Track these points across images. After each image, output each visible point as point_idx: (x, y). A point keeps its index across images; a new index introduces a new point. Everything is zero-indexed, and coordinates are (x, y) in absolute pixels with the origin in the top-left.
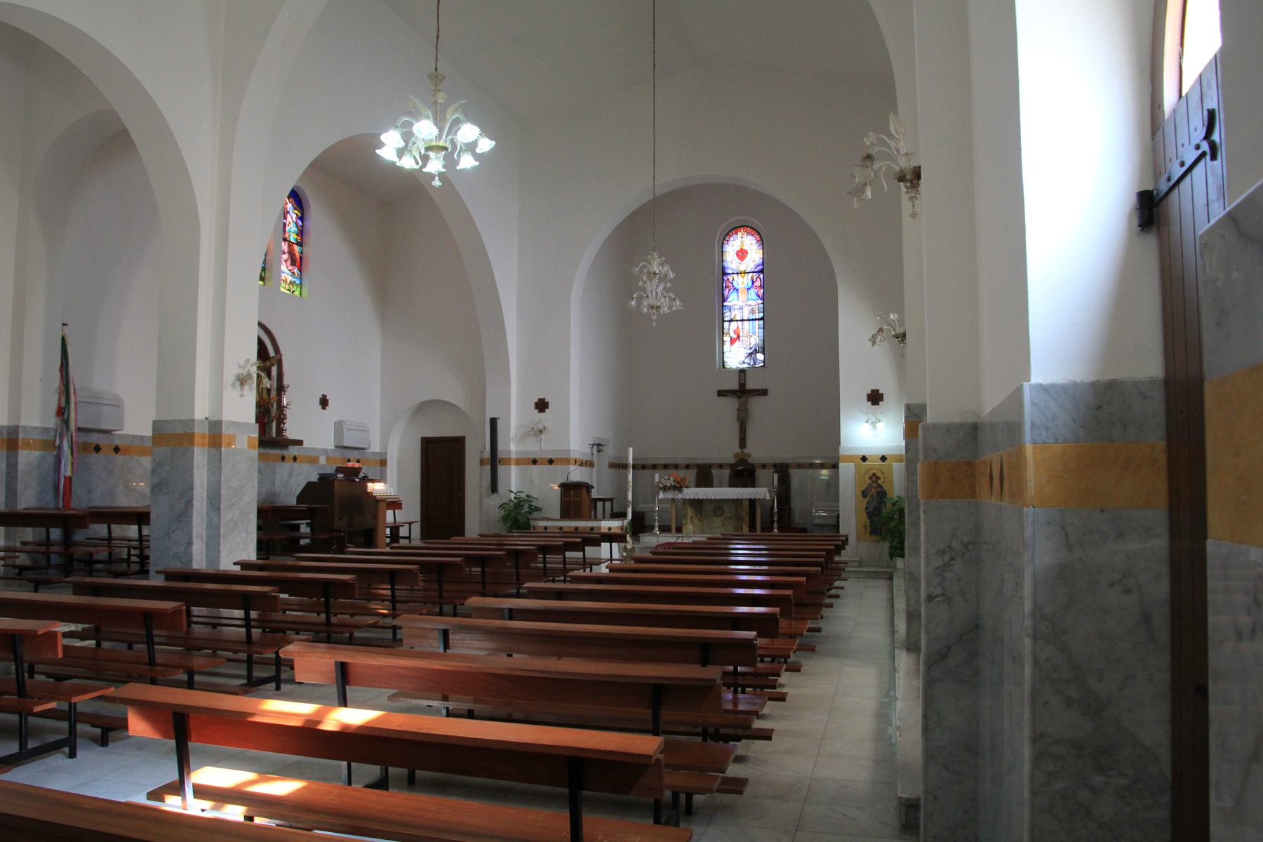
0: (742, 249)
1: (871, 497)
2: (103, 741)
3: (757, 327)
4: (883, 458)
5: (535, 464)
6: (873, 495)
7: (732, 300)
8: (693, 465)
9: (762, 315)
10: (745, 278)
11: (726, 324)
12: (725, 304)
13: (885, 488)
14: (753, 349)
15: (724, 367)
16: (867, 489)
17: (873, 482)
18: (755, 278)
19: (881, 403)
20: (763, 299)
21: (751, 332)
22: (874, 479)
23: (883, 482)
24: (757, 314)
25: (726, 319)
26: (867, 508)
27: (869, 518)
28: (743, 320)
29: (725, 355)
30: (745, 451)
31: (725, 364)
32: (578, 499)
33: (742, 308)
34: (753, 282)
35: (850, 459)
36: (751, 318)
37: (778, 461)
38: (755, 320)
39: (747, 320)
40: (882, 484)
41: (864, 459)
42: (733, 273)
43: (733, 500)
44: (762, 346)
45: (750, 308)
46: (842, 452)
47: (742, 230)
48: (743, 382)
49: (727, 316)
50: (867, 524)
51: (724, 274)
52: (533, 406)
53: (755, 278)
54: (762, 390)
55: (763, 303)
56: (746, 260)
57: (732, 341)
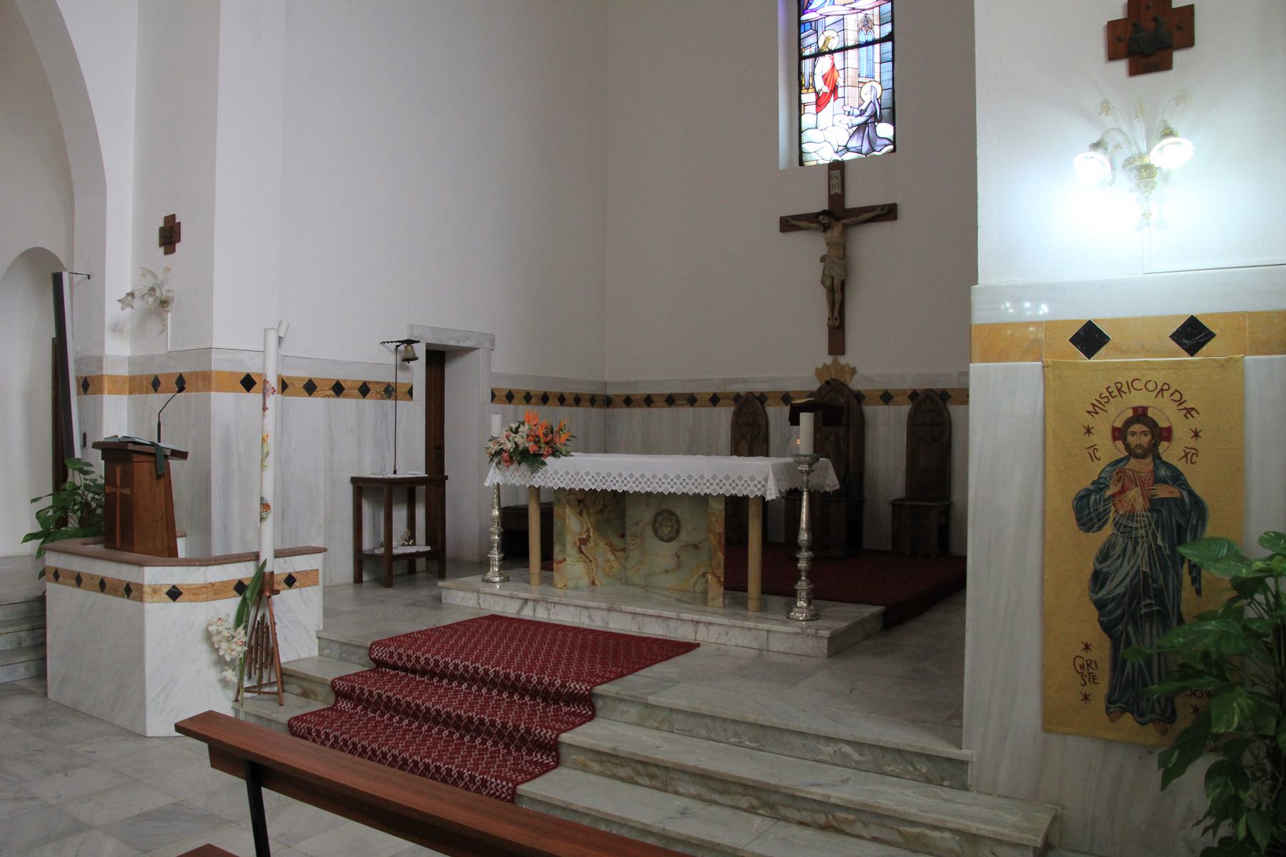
2: (180, 727)
3: (877, 59)
6: (1131, 515)
8: (726, 396)
9: (887, 29)
11: (807, 64)
12: (804, 18)
13: (1197, 489)
15: (801, 163)
16: (1100, 485)
17: (1132, 453)
22: (1139, 436)
23: (1189, 456)
25: (807, 52)
26: (1098, 579)
27: (1107, 627)
29: (805, 137)
30: (843, 360)
31: (806, 157)
36: (863, 39)
37: (920, 386)
38: (873, 42)
40: (1181, 466)
44: (887, 100)
45: (861, 15)
46: (981, 314)
48: (839, 191)
50: (1093, 654)
54: (883, 207)
57: (820, 103)
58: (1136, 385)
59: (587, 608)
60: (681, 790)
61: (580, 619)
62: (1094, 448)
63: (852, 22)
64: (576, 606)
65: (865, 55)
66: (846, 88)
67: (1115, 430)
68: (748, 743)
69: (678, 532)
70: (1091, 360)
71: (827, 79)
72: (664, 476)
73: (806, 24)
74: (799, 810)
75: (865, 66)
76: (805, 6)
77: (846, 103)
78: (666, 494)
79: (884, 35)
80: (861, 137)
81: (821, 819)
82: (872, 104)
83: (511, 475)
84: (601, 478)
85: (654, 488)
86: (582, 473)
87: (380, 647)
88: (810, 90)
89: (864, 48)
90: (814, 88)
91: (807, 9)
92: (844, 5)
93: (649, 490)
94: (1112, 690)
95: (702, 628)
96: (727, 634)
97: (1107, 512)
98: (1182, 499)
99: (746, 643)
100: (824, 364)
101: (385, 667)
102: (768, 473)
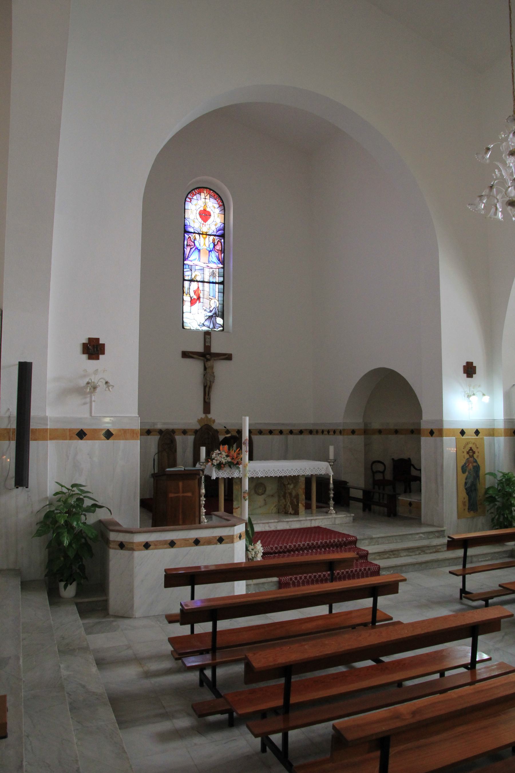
0: (205, 210)
1: (469, 472)
3: (217, 290)
4: (477, 432)
5: (81, 438)
6: (470, 470)
7: (193, 259)
8: (155, 430)
9: (221, 279)
10: (207, 239)
11: (186, 284)
12: (185, 262)
14: (213, 312)
16: (465, 464)
19: (474, 375)
20: (223, 263)
21: (212, 295)
22: (471, 454)
26: (466, 483)
27: (468, 494)
28: (203, 282)
30: (209, 416)
32: (189, 494)
33: (203, 269)
34: (214, 245)
35: (451, 432)
36: (211, 280)
38: (216, 283)
39: (207, 282)
41: (463, 433)
42: (194, 233)
43: (276, 477)
45: (211, 270)
46: (446, 426)
49: (188, 275)
51: (186, 232)
52: (79, 349)
55: (223, 268)
56: (210, 221)
57: (193, 302)
58: (470, 442)
59: (268, 523)
60: (402, 555)
61: (265, 528)
62: (464, 456)
63: (207, 272)
64: (263, 523)
65: (212, 287)
66: (204, 299)
67: (467, 452)
68: (399, 541)
69: (265, 491)
70: (463, 437)
72: (291, 470)
74: (430, 550)
75: (212, 291)
76: (186, 258)
77: (204, 305)
78: (260, 477)
79: (220, 282)
80: (210, 322)
81: (434, 550)
82: (214, 309)
83: (222, 474)
84: (293, 471)
85: (292, 474)
86: (257, 470)
87: (267, 547)
89: (212, 284)
90: (190, 295)
91: (187, 259)
92: (204, 263)
93: (285, 475)
94: (469, 507)
95: (313, 521)
96: (322, 522)
97: (466, 469)
98: (477, 466)
99: (328, 523)
100: (201, 418)
101: (266, 555)
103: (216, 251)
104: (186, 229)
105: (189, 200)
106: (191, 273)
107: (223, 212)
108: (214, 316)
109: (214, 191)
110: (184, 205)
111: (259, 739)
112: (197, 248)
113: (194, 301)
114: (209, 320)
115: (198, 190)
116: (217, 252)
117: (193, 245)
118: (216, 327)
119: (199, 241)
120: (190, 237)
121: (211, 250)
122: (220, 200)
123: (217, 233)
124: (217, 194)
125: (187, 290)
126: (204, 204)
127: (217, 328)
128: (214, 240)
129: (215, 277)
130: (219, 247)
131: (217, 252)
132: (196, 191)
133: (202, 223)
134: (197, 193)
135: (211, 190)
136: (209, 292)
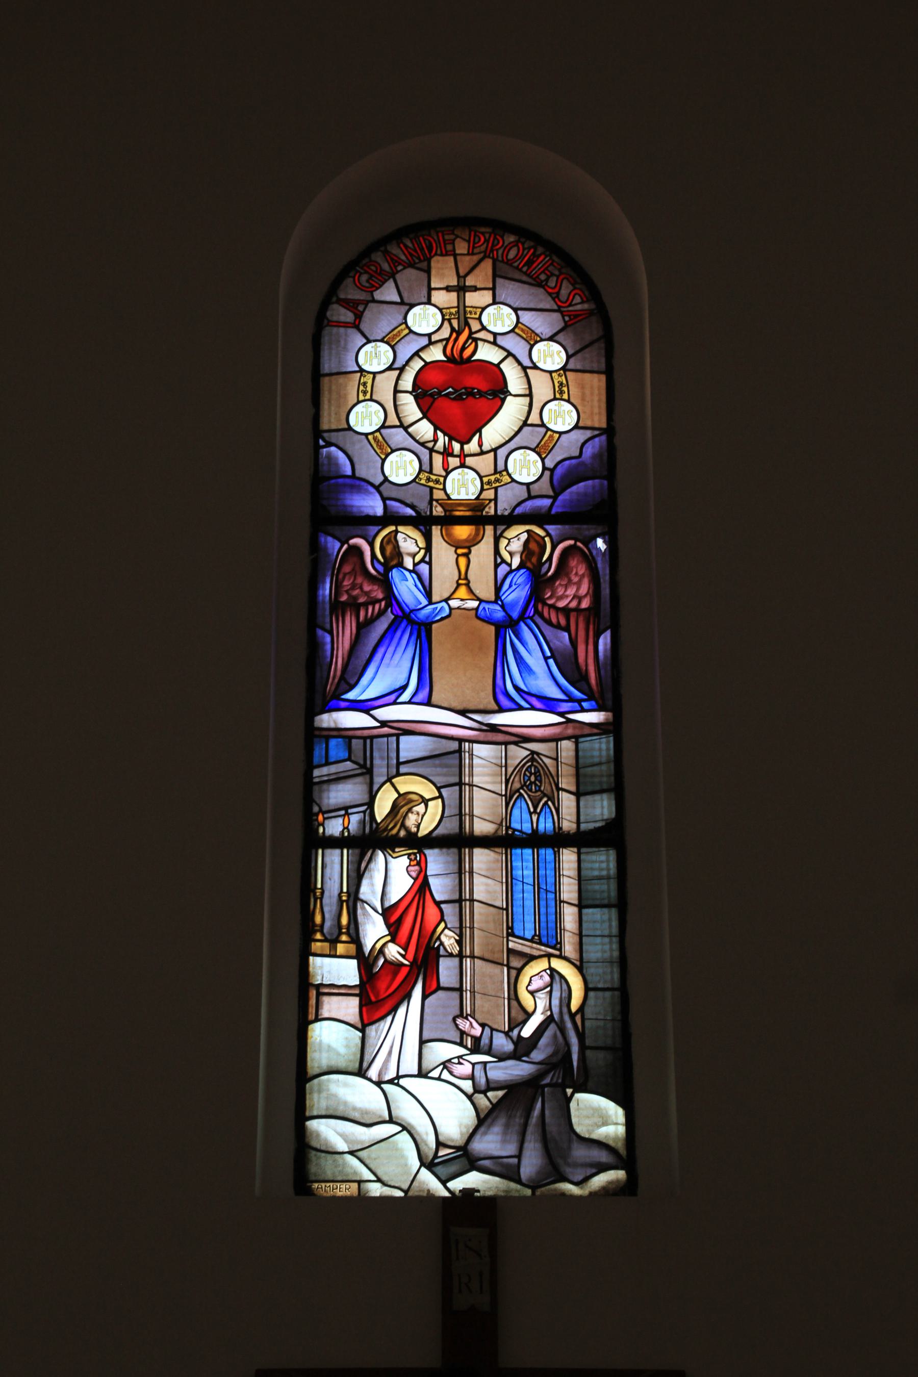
3: (569, 890)
10: (483, 552)
12: (327, 720)
18: (552, 555)
24: (567, 802)
25: (334, 827)
36: (522, 821)
39: (486, 842)
45: (519, 754)
47: (461, 247)
53: (552, 555)
65: (528, 873)
71: (400, 921)
73: (333, 743)
75: (529, 903)
79: (591, 826)
80: (516, 1128)
82: (552, 1028)
88: (341, 948)
102: (570, 596)
103: (549, 622)
104: (325, 503)
105: (349, 317)
106: (365, 788)
107: (594, 356)
108: (547, 1080)
109: (523, 233)
110: (310, 353)
111: (393, 617)
112: (378, 430)
113: (384, 987)
114: (510, 1118)
115: (409, 244)
116: (563, 622)
117: (374, 602)
118: (568, 1171)
119: (424, 568)
120: (357, 551)
121: (515, 615)
122: (573, 284)
123: (555, 498)
124: (553, 248)
125: (335, 908)
126: (455, 323)
127: (579, 1178)
128: (532, 549)
129: (551, 798)
130: (571, 591)
131: (558, 627)
132: (395, 250)
133: (440, 445)
134: (400, 262)
135: (500, 227)
136: (508, 909)
